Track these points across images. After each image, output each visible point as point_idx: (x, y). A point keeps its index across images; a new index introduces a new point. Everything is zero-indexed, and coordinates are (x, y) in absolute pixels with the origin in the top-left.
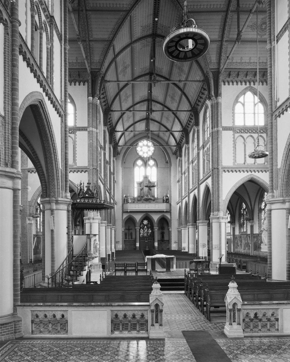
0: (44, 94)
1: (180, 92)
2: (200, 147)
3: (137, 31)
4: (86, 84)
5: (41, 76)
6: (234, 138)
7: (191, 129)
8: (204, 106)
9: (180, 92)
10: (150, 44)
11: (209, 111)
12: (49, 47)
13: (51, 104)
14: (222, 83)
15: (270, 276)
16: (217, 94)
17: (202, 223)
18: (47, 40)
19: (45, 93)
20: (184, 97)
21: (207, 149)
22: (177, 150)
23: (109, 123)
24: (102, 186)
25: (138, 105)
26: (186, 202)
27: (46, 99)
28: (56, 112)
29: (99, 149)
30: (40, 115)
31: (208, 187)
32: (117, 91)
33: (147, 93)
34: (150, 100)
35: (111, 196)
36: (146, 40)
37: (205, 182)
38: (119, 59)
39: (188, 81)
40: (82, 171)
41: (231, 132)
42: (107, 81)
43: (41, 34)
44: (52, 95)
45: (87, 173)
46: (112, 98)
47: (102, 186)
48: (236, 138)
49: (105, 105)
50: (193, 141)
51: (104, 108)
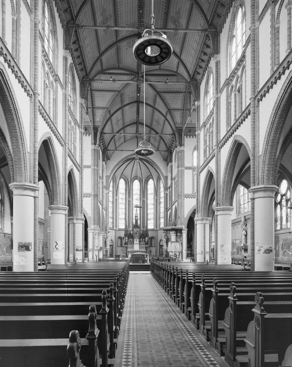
0: (6, 65)
1: (163, 118)
2: (201, 125)
3: (123, 50)
4: (91, 135)
5: (16, 67)
6: (193, 174)
7: (174, 150)
8: (207, 72)
9: (163, 118)
10: (136, 106)
11: (213, 77)
12: (15, 18)
13: (12, 73)
14: (185, 136)
15: (254, 270)
16: (181, 144)
17: (265, 191)
18: (12, 10)
19: (6, 64)
20: (162, 141)
21: (210, 124)
22: (168, 155)
23: (102, 143)
24: (100, 206)
25: (128, 127)
26: (176, 207)
27: (53, 135)
28: (43, 119)
29: (99, 179)
30: (51, 155)
31: (211, 173)
32: (98, 55)
33: (136, 117)
34: (138, 123)
35: (103, 206)
36: (132, 39)
37: (207, 167)
38: (113, 118)
39: (163, 134)
40: (87, 196)
41: (191, 171)
42: (104, 133)
43: (49, 91)
44: (57, 133)
45: (90, 197)
46: (108, 142)
47: (100, 206)
48: (194, 174)
49: (103, 146)
50: (206, 92)
51: (102, 148)
